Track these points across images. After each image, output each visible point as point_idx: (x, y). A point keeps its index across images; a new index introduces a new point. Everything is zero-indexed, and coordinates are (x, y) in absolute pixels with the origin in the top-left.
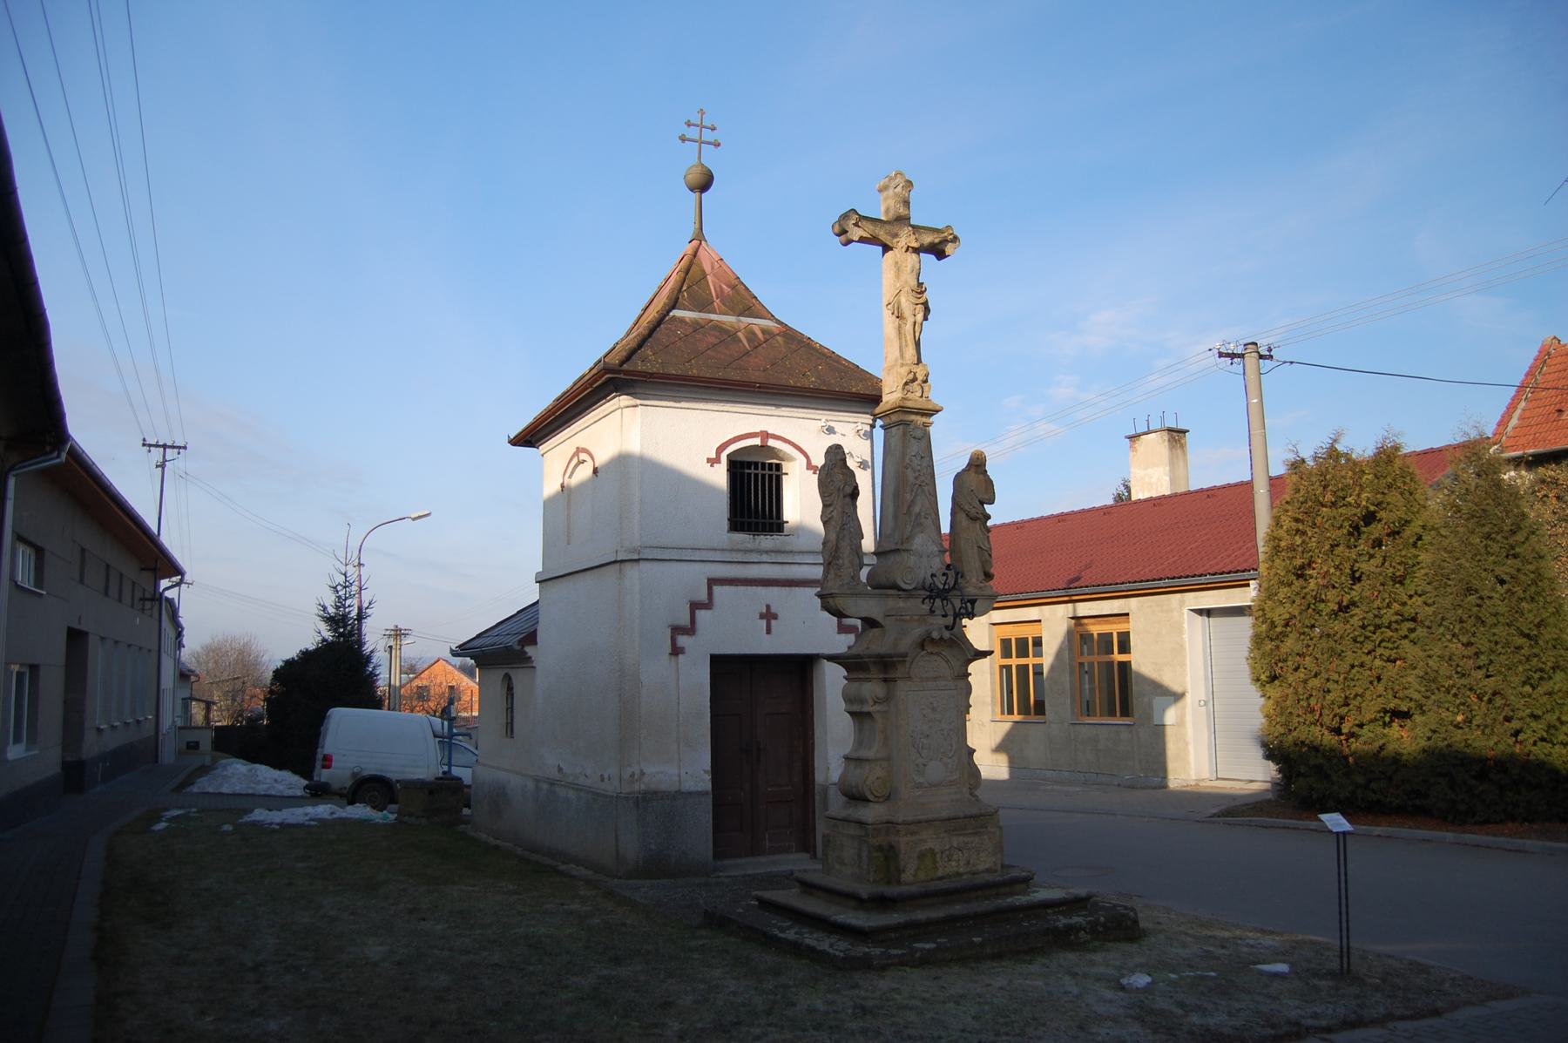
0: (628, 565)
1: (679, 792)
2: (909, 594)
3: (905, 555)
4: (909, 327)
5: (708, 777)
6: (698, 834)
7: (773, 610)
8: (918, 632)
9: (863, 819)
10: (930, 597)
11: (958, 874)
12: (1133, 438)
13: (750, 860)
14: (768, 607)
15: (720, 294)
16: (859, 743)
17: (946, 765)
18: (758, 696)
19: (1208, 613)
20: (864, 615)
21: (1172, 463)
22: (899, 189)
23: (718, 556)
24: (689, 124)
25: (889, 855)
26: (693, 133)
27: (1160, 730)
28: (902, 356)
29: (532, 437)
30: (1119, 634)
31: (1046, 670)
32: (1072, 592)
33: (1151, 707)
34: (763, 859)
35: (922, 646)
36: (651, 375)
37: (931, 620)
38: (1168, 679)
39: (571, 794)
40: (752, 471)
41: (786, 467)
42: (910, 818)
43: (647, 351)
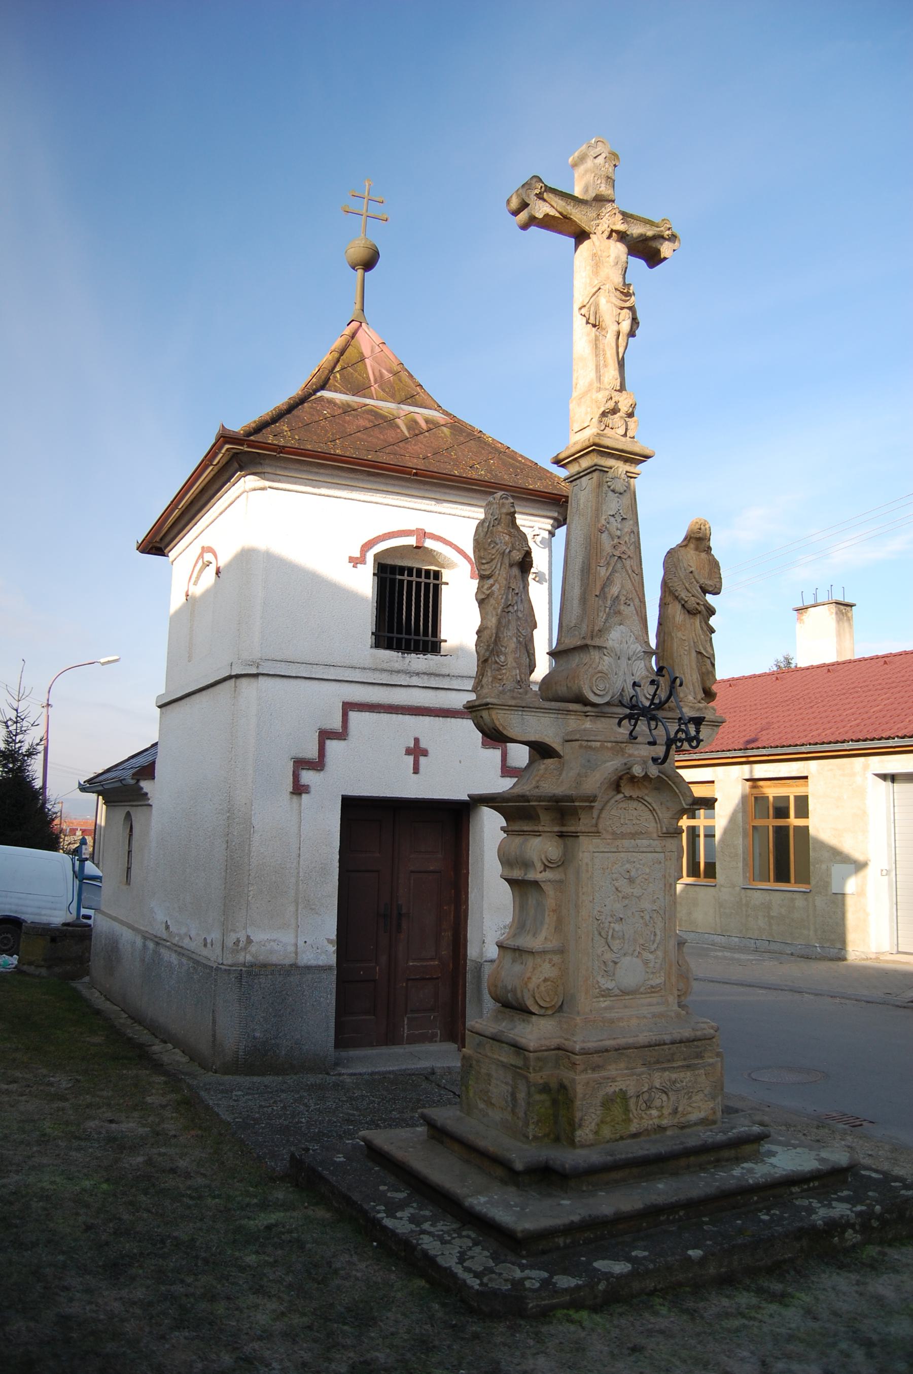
0: (244, 682)
1: (294, 966)
2: (599, 711)
3: (595, 654)
4: (610, 337)
5: (333, 949)
6: (316, 1018)
7: (423, 745)
8: (611, 765)
9: (523, 1041)
10: (629, 717)
11: (661, 1129)
12: (801, 610)
13: (384, 1050)
14: (417, 740)
15: (380, 379)
16: (521, 925)
17: (646, 963)
18: (398, 849)
19: (892, 778)
20: (532, 738)
21: (839, 634)
22: (600, 160)
23: (358, 676)
25: (560, 1097)
27: (839, 899)
28: (599, 378)
29: (157, 543)
30: (796, 797)
31: (718, 834)
32: (750, 753)
33: (829, 875)
34: (398, 1050)
35: (617, 786)
36: (282, 449)
37: (631, 750)
38: (848, 845)
39: (174, 958)
40: (405, 577)
41: (446, 575)
42: (591, 1045)
43: (283, 426)
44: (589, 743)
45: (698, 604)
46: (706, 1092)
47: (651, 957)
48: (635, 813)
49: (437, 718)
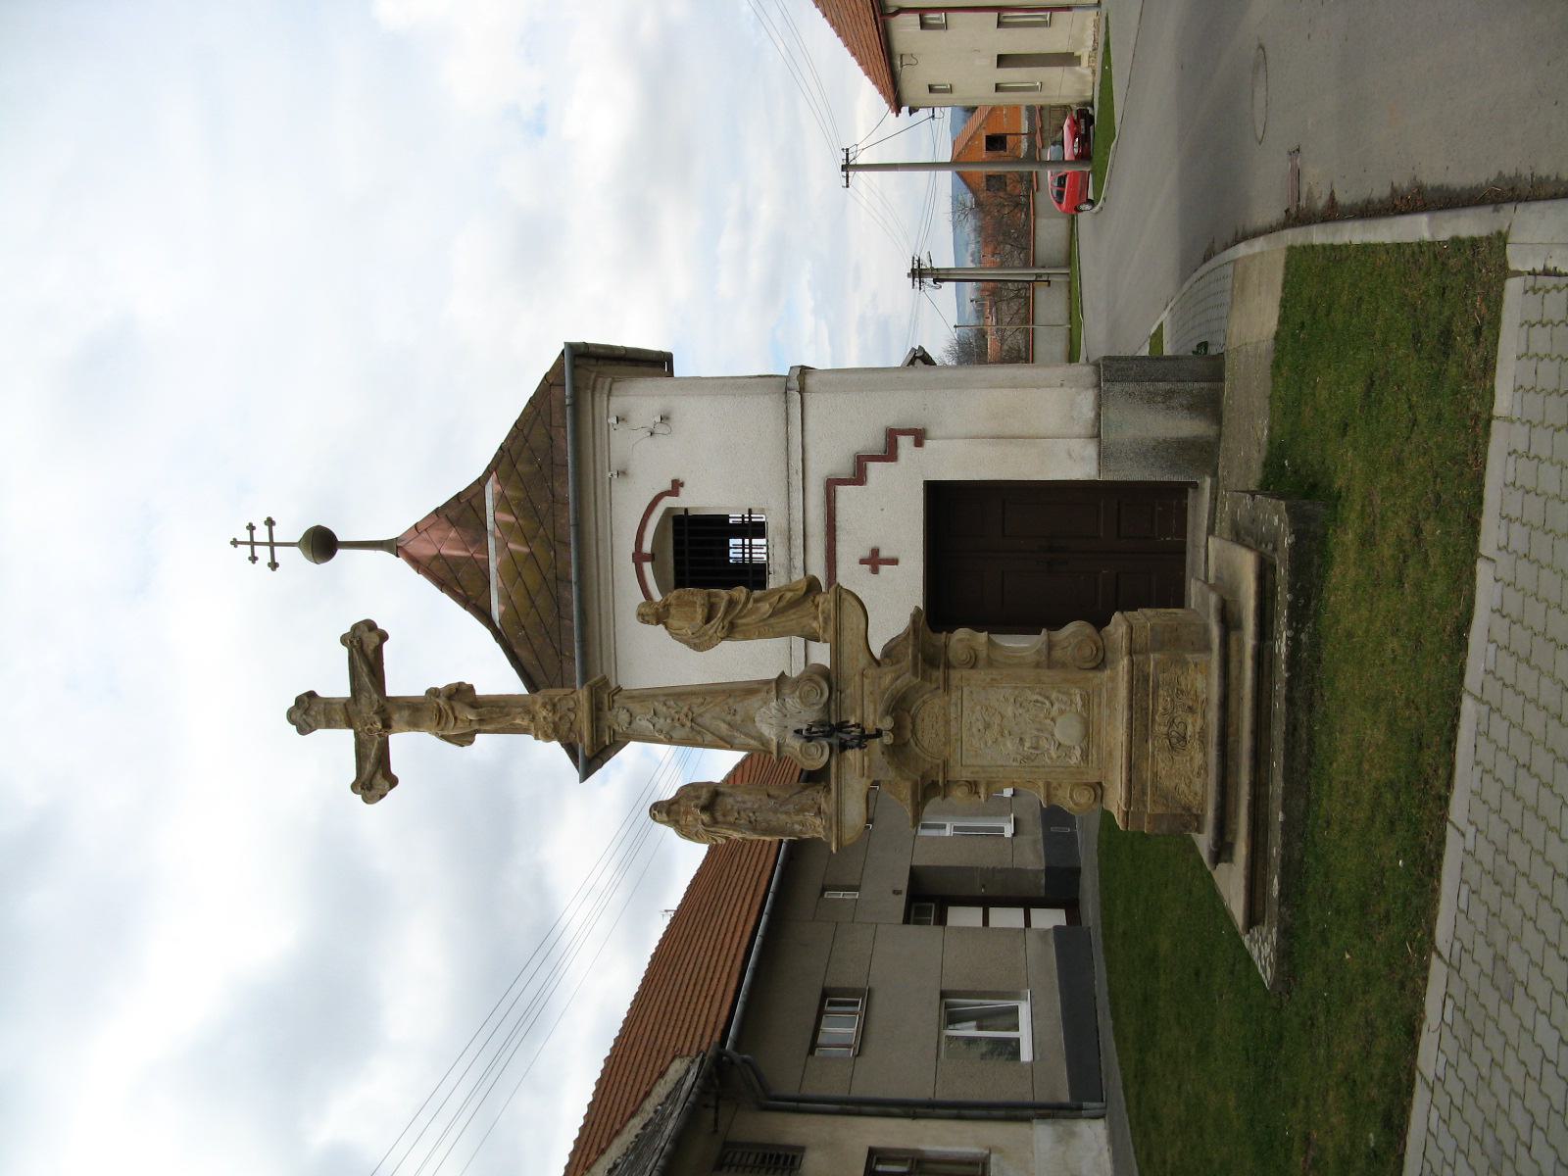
7: (867, 554)
14: (862, 562)
17: (1062, 712)
24: (254, 559)
26: (263, 553)
44: (866, 767)
45: (723, 628)
46: (1179, 672)
47: (1056, 707)
48: (927, 719)
49: (837, 538)
